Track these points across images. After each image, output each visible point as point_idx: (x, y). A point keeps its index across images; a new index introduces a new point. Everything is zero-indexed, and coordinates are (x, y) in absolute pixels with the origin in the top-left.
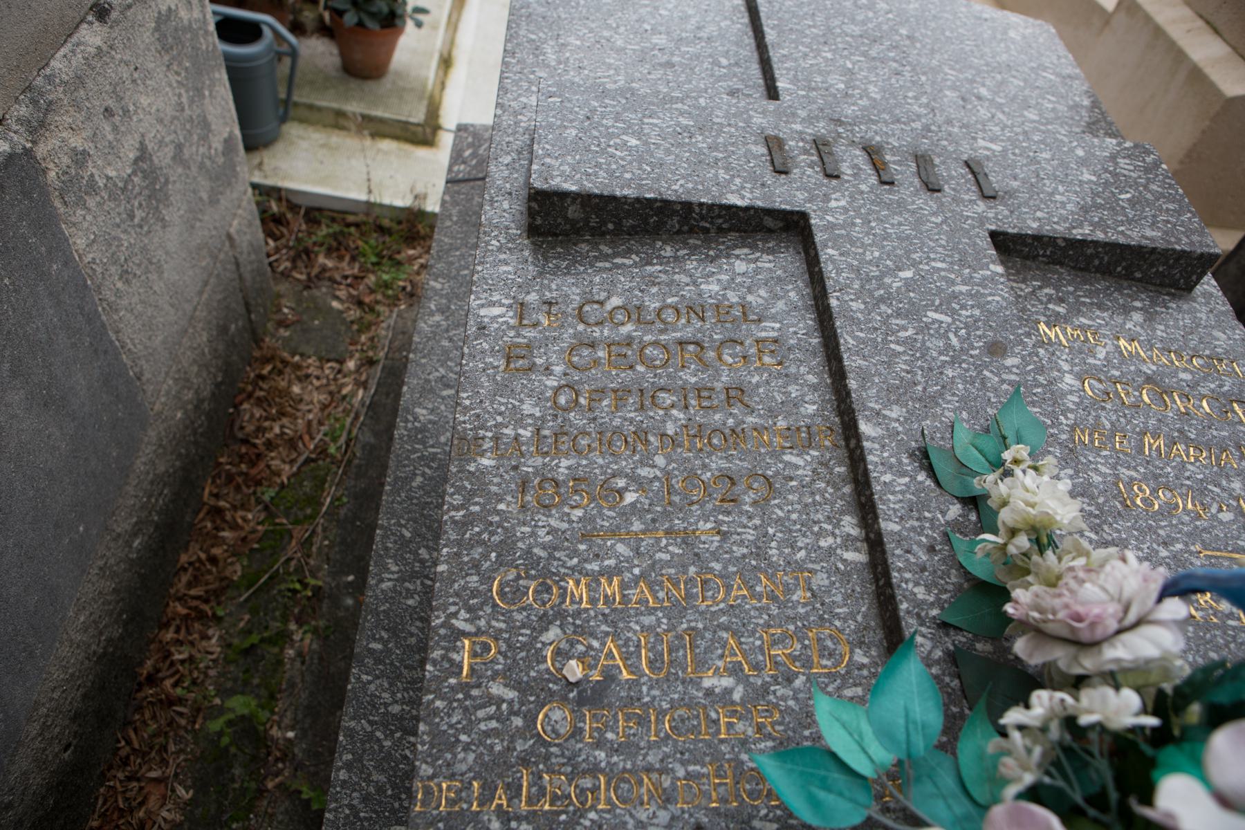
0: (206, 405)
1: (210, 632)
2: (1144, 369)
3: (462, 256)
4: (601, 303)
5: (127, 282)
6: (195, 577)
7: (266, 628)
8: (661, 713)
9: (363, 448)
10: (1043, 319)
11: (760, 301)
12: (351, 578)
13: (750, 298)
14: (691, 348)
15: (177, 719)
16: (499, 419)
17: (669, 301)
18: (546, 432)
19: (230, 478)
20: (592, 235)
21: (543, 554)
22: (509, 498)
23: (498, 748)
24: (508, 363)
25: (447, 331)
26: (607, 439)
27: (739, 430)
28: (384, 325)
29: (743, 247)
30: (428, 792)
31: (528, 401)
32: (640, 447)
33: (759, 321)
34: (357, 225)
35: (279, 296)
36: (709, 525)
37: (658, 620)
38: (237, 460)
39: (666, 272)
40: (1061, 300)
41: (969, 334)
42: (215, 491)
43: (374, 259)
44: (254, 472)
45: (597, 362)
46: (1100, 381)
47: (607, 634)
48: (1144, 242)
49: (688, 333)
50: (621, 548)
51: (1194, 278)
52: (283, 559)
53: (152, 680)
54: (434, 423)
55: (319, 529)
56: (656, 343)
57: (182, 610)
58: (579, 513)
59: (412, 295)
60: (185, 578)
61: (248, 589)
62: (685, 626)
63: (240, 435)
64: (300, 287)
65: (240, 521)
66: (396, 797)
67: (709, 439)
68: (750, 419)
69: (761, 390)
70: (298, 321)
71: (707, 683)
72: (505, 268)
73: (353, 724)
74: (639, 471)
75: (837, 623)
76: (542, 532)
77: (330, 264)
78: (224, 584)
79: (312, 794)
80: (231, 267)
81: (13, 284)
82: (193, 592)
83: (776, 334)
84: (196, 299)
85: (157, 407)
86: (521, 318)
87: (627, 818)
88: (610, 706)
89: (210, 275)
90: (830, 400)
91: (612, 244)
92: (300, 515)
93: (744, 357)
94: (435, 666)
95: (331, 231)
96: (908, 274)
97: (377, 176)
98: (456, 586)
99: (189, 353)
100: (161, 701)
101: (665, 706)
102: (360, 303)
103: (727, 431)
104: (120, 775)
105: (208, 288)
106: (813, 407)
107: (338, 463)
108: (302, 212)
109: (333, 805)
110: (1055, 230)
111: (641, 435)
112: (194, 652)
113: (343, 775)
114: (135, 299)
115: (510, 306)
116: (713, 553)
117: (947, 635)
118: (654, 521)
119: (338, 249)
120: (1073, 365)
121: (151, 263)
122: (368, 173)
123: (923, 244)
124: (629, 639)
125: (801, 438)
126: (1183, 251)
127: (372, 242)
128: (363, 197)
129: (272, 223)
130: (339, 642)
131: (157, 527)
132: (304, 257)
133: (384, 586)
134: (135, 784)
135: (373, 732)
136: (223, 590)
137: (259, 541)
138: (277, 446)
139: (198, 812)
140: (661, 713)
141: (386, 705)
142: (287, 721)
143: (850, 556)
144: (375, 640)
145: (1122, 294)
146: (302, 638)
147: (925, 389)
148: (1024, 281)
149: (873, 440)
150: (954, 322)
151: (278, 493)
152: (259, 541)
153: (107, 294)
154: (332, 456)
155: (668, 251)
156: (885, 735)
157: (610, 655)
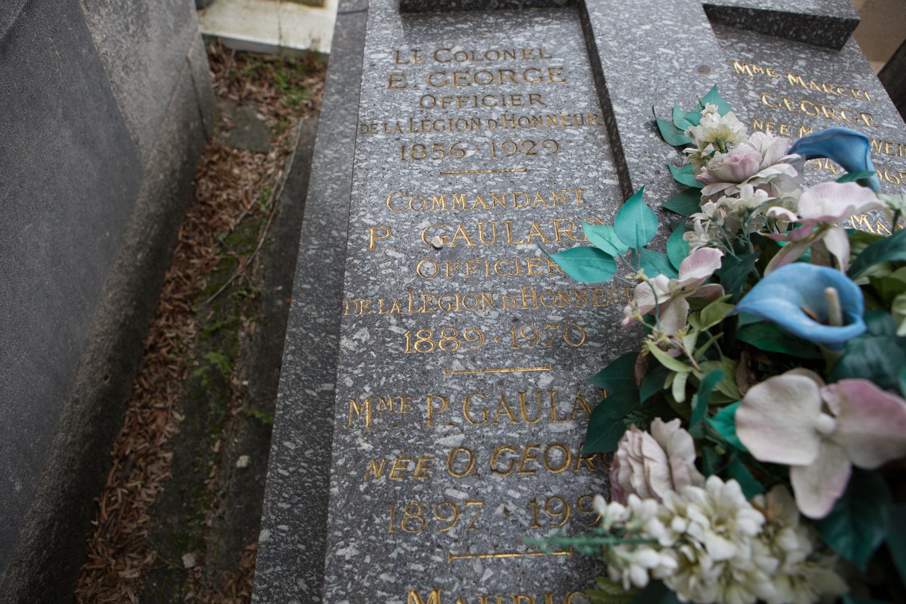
0: (177, 175)
1: (189, 322)
2: (804, 92)
3: (351, 59)
4: (449, 50)
5: (127, 73)
6: (177, 287)
7: (225, 319)
8: (492, 263)
9: (284, 207)
10: (737, 60)
11: (551, 46)
12: (280, 288)
13: (544, 45)
14: (507, 73)
15: (172, 373)
16: (387, 114)
17: (493, 47)
18: (416, 120)
19: (195, 226)
20: (442, 11)
21: (417, 184)
22: (395, 155)
23: (393, 283)
24: (390, 84)
25: (343, 104)
26: (454, 124)
27: (537, 116)
28: (294, 129)
29: (540, 16)
30: (352, 306)
31: (404, 104)
32: (475, 126)
33: (551, 57)
34: (272, 62)
35: (220, 110)
36: (519, 167)
37: (489, 216)
38: (199, 215)
39: (490, 32)
40: (750, 51)
41: (686, 61)
42: (186, 234)
43: (285, 85)
44: (211, 222)
45: (446, 82)
46: (773, 97)
47: (458, 223)
48: (808, 12)
49: (505, 65)
50: (465, 179)
51: (842, 39)
52: (233, 277)
53: (153, 348)
54: (338, 159)
55: (257, 258)
56: (484, 71)
57: (169, 307)
58: (439, 162)
59: (312, 109)
60: (170, 288)
61: (211, 295)
63: (200, 199)
64: (233, 105)
65: (204, 253)
67: (519, 121)
68: (545, 111)
69: (552, 95)
70: (235, 127)
71: (519, 247)
72: (386, 32)
73: (294, 330)
74: (475, 139)
75: (599, 216)
76: (416, 172)
77: (254, 89)
78: (196, 292)
79: (262, 415)
80: (189, 81)
81: (61, 55)
82: (176, 296)
83: (561, 65)
84: (169, 98)
85: (148, 166)
86: (398, 59)
87: (473, 315)
88: (461, 260)
89: (177, 83)
90: (596, 100)
91: (455, 16)
92: (244, 249)
93: (541, 78)
94: (352, 242)
95: (254, 66)
96: (648, 27)
97: (285, 27)
98: (364, 201)
99: (166, 135)
100: (160, 361)
101: (494, 259)
102: (277, 115)
103: (530, 118)
104: (138, 404)
105: (176, 93)
106: (583, 99)
107: (267, 218)
108: (233, 53)
109: (285, 374)
110: (747, 5)
111: (476, 121)
112: (179, 333)
113: (289, 357)
114: (132, 87)
115: (391, 53)
116: (523, 181)
117: (666, 215)
118: (485, 165)
119: (260, 79)
120: (755, 86)
121: (141, 64)
122: (279, 23)
123: (658, 10)
124: (471, 226)
125: (579, 120)
126: (835, 18)
127: (284, 73)
128: (275, 42)
129: (214, 59)
130: (275, 325)
131: (151, 250)
132: (236, 84)
133: (310, 252)
134: (147, 410)
135: (307, 334)
136: (196, 296)
137: (217, 266)
138: (226, 207)
139: (189, 428)
140: (492, 263)
141: (315, 319)
142: (242, 375)
143: (607, 181)
144: (305, 283)
145: (792, 50)
146: (249, 325)
147: (656, 90)
148: (726, 38)
149: (622, 115)
150: (676, 54)
151: (228, 236)
153: (116, 79)
154: (264, 214)
155: (491, 20)
156: (623, 237)
157: (460, 234)
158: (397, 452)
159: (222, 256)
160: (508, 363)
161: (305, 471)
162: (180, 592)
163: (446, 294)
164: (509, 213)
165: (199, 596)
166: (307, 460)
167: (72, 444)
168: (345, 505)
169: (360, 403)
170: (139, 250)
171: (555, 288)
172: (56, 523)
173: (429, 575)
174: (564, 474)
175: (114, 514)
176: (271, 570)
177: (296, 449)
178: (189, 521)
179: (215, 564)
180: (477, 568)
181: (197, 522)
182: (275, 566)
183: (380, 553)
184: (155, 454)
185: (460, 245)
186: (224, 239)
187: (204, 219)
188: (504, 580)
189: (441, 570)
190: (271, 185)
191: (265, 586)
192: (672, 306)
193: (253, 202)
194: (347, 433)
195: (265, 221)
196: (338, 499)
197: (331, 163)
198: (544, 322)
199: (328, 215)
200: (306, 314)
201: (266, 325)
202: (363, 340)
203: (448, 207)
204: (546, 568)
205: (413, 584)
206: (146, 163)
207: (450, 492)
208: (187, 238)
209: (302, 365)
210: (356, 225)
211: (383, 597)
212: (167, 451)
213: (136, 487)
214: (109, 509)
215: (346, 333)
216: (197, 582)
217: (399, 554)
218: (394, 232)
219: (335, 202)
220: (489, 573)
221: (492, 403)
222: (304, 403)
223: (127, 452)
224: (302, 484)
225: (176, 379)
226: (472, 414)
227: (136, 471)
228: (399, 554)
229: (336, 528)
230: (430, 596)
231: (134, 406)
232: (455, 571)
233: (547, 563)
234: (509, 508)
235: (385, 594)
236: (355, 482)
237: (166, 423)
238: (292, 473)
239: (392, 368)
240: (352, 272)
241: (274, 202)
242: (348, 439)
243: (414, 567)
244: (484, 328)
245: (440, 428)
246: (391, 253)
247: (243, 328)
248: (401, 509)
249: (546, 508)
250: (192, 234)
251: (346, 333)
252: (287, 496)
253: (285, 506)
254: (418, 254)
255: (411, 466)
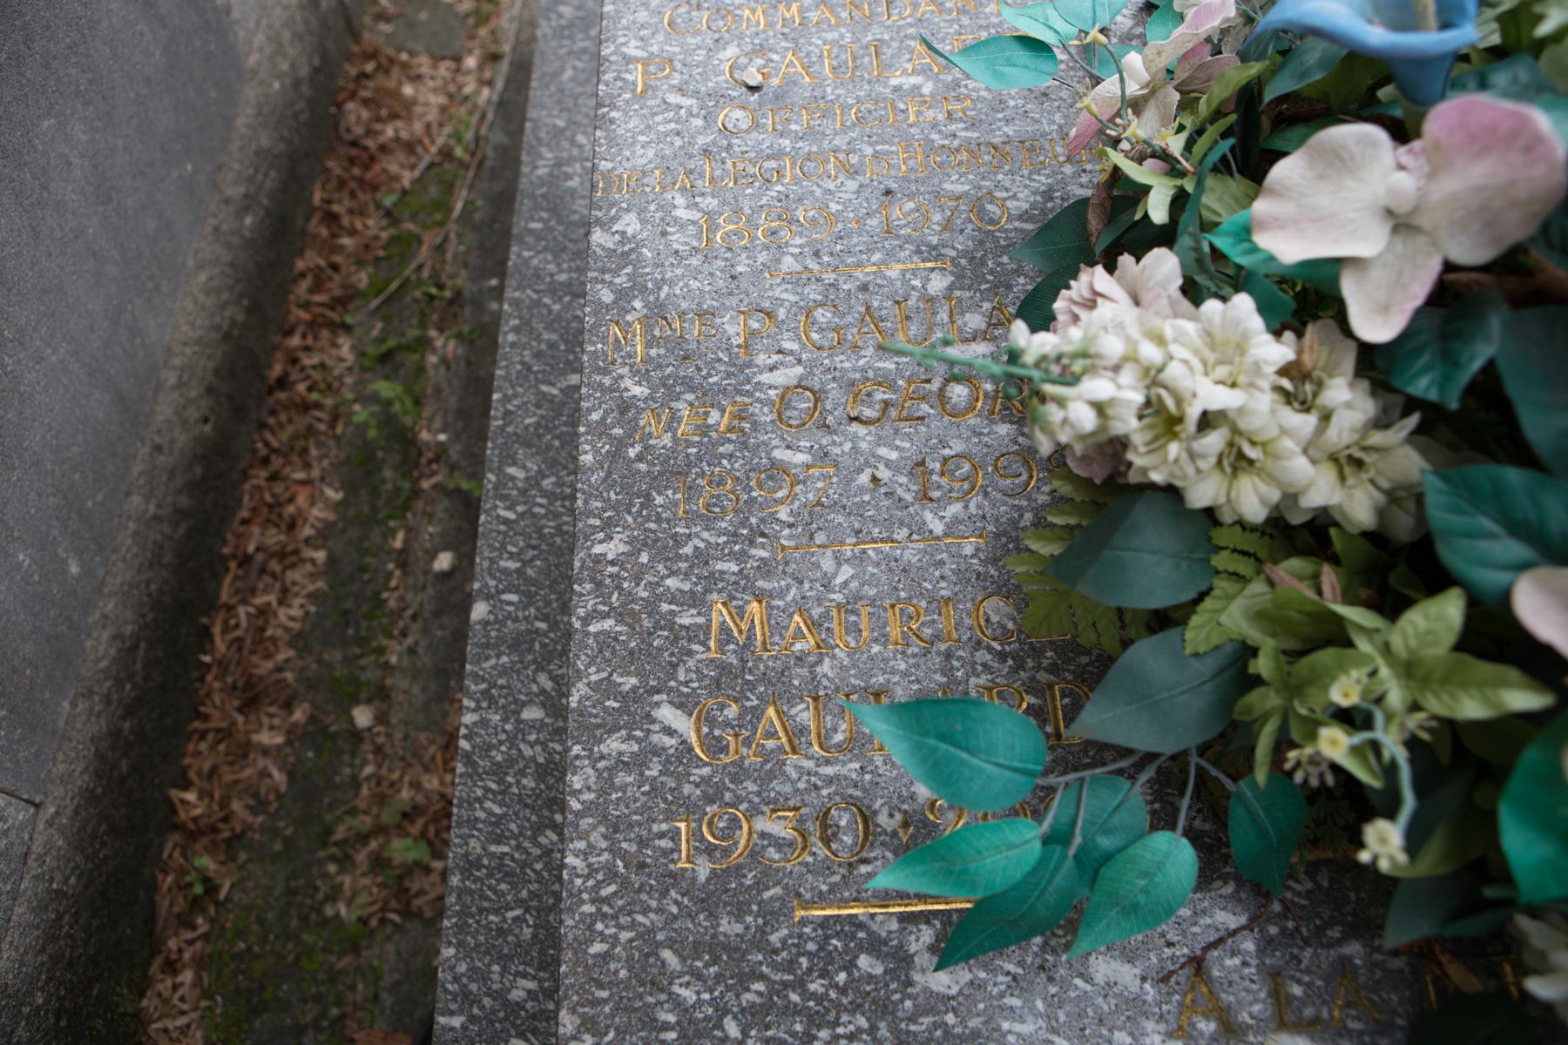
8: (845, 108)
9: (496, 148)
19: (342, 184)
42: (326, 196)
47: (787, 49)
52: (413, 265)
53: (282, 383)
55: (453, 236)
62: (870, 38)
63: (348, 137)
66: (568, 351)
70: (400, 15)
71: (894, 82)
73: (517, 294)
82: (317, 298)
92: (429, 221)
98: (624, 22)
100: (295, 405)
101: (850, 101)
107: (466, 166)
109: (503, 363)
113: (511, 337)
133: (540, 172)
135: (539, 300)
136: (351, 298)
137: (385, 247)
139: (351, 512)
140: (845, 108)
141: (552, 275)
146: (445, 345)
151: (400, 200)
152: (385, 247)
158: (690, 397)
159: (392, 231)
160: (876, 257)
161: (543, 511)
162: (352, 766)
163: (769, 158)
164: (875, 29)
165: (384, 771)
166: (545, 494)
167: (156, 518)
168: (604, 480)
169: (626, 328)
170: (246, 209)
171: (956, 143)
172: (143, 645)
173: (746, 577)
174: (972, 422)
175: (234, 647)
176: (493, 662)
177: (527, 479)
178: (359, 657)
179: (406, 723)
180: (827, 564)
181: (373, 658)
182: (498, 656)
183: (665, 548)
184: (296, 552)
185: (790, 82)
186: (395, 205)
187: (356, 171)
188: (873, 581)
189: (765, 569)
190: (470, 113)
191: (484, 686)
192: (1152, 103)
193: (440, 141)
194: (605, 372)
195: (462, 172)
196: (592, 470)
197: (571, 25)
198: (937, 194)
199: (569, 111)
200: (536, 268)
201: (472, 342)
202: (630, 232)
203: (769, 25)
204: (942, 563)
205: (720, 591)
206: (248, 55)
207: (780, 454)
208: (329, 202)
209: (532, 348)
210: (613, 58)
211: (672, 612)
212: (316, 548)
213: (269, 604)
214: (229, 637)
215: (598, 222)
216: (378, 750)
217: (696, 548)
218: (678, 66)
219: (580, 89)
220: (847, 572)
221: (849, 319)
222: (538, 406)
223: (251, 549)
224: (539, 531)
225: (325, 434)
226: (815, 336)
227: (267, 579)
228: (696, 548)
229: (590, 514)
230: (749, 608)
231: (256, 477)
232: (789, 570)
233: (944, 555)
234: (879, 475)
235: (673, 607)
236: (621, 444)
237: (313, 504)
238: (522, 515)
239: (679, 272)
240: (608, 130)
241: (477, 139)
242: (607, 381)
243: (720, 566)
244: (834, 207)
245: (761, 359)
246: (673, 99)
247: (434, 350)
248: (699, 481)
249: (942, 474)
250: (336, 196)
251: (598, 222)
252: (514, 550)
253: (512, 565)
254: (720, 98)
255: (714, 416)
